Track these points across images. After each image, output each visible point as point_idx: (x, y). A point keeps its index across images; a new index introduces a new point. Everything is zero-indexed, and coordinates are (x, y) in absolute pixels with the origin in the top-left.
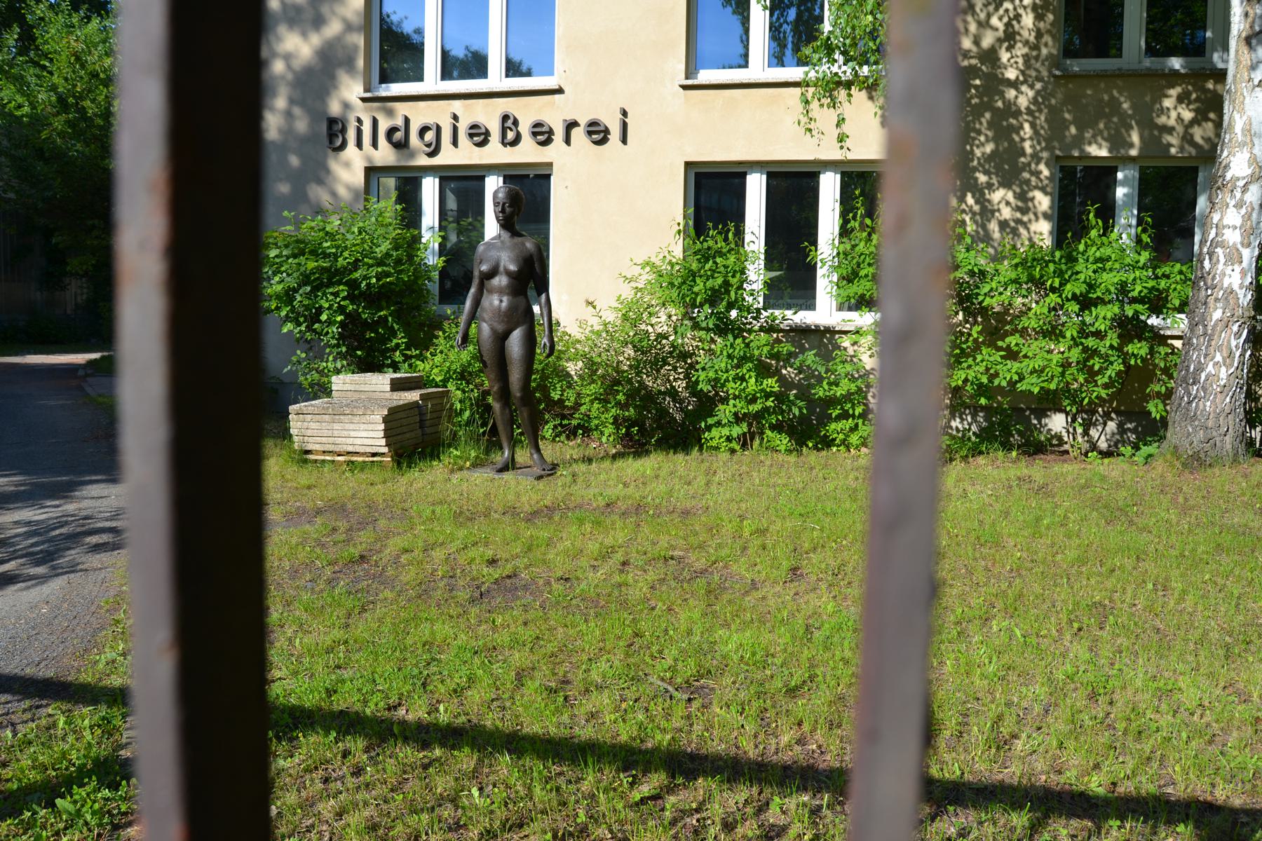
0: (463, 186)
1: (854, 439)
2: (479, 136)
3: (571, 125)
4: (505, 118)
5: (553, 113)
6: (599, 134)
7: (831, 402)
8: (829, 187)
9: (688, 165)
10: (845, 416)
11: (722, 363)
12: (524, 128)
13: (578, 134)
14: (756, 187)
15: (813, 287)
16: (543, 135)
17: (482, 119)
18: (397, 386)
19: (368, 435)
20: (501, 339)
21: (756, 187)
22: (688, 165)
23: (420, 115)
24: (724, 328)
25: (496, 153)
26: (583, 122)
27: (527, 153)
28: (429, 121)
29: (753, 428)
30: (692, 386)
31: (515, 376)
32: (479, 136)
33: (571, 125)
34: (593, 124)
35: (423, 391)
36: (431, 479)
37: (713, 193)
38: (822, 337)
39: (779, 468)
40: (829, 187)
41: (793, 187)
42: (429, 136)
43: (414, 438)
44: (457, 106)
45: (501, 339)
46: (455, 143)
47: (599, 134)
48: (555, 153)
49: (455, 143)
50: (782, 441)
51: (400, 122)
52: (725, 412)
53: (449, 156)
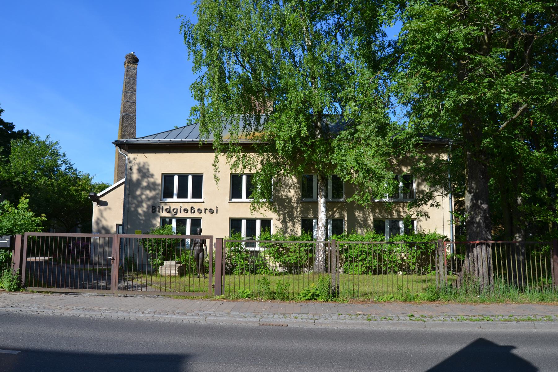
0: (181, 222)
1: (262, 273)
2: (186, 211)
3: (206, 210)
4: (192, 207)
5: (202, 207)
6: (211, 211)
7: (257, 266)
8: (258, 223)
9: (162, 174)
10: (260, 268)
11: (237, 258)
12: (196, 210)
13: (207, 211)
14: (244, 223)
15: (82, 233)
16: (200, 211)
17: (186, 207)
18: (177, 263)
19: (174, 271)
20: (198, 254)
21: (244, 223)
22: (162, 174)
23: (173, 206)
24: (238, 251)
25: (189, 215)
26: (208, 209)
27: (196, 215)
28: (175, 207)
29: (242, 271)
30: (231, 263)
31: (200, 261)
32: (186, 211)
33: (206, 210)
34: (210, 209)
35: (253, 249)
36: (188, 279)
37: (235, 224)
38: (257, 253)
39: (248, 278)
40: (258, 223)
41: (251, 223)
42: (175, 211)
43: (182, 272)
44: (181, 204)
45: (198, 254)
46: (181, 212)
47: (211, 211)
48: (202, 215)
49: (181, 212)
50: (248, 273)
51: (168, 207)
52: (238, 267)
53: (179, 215)
